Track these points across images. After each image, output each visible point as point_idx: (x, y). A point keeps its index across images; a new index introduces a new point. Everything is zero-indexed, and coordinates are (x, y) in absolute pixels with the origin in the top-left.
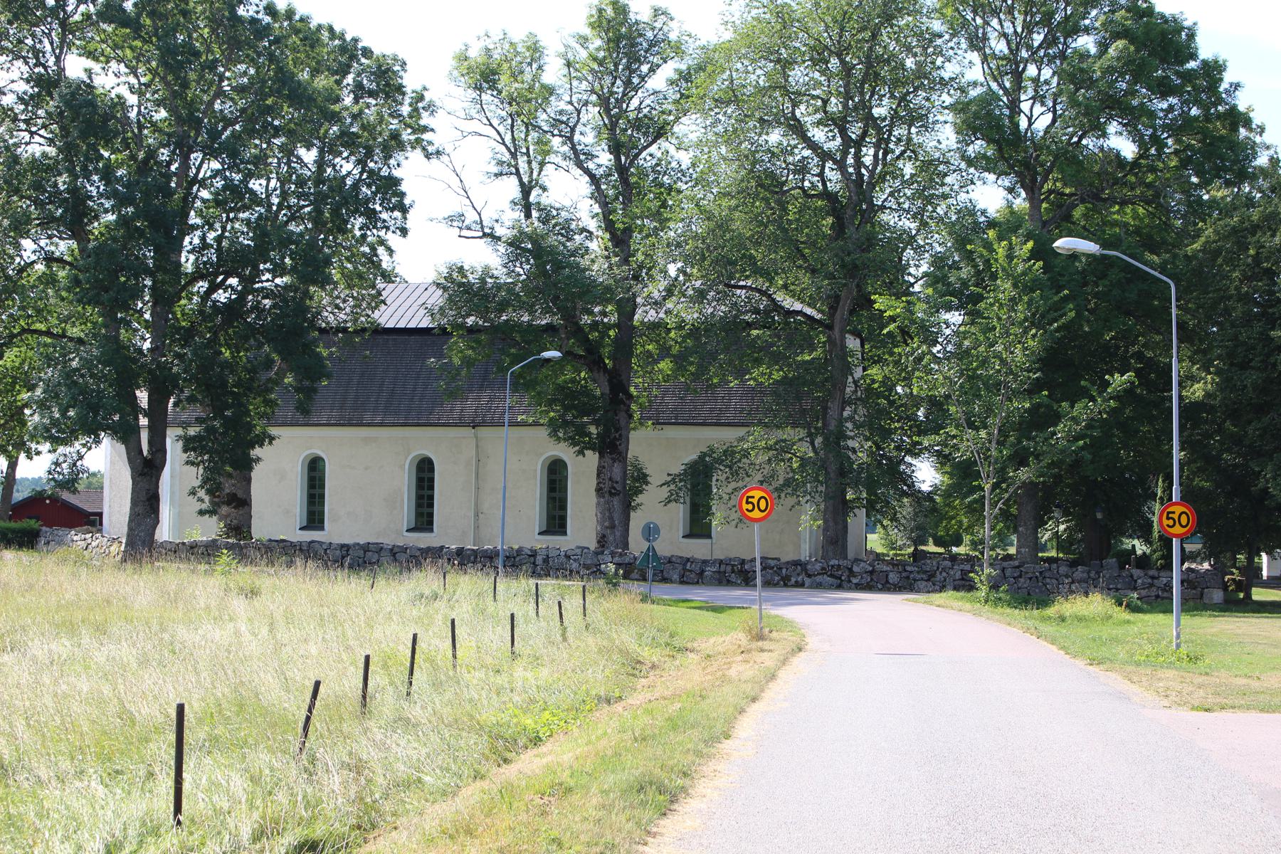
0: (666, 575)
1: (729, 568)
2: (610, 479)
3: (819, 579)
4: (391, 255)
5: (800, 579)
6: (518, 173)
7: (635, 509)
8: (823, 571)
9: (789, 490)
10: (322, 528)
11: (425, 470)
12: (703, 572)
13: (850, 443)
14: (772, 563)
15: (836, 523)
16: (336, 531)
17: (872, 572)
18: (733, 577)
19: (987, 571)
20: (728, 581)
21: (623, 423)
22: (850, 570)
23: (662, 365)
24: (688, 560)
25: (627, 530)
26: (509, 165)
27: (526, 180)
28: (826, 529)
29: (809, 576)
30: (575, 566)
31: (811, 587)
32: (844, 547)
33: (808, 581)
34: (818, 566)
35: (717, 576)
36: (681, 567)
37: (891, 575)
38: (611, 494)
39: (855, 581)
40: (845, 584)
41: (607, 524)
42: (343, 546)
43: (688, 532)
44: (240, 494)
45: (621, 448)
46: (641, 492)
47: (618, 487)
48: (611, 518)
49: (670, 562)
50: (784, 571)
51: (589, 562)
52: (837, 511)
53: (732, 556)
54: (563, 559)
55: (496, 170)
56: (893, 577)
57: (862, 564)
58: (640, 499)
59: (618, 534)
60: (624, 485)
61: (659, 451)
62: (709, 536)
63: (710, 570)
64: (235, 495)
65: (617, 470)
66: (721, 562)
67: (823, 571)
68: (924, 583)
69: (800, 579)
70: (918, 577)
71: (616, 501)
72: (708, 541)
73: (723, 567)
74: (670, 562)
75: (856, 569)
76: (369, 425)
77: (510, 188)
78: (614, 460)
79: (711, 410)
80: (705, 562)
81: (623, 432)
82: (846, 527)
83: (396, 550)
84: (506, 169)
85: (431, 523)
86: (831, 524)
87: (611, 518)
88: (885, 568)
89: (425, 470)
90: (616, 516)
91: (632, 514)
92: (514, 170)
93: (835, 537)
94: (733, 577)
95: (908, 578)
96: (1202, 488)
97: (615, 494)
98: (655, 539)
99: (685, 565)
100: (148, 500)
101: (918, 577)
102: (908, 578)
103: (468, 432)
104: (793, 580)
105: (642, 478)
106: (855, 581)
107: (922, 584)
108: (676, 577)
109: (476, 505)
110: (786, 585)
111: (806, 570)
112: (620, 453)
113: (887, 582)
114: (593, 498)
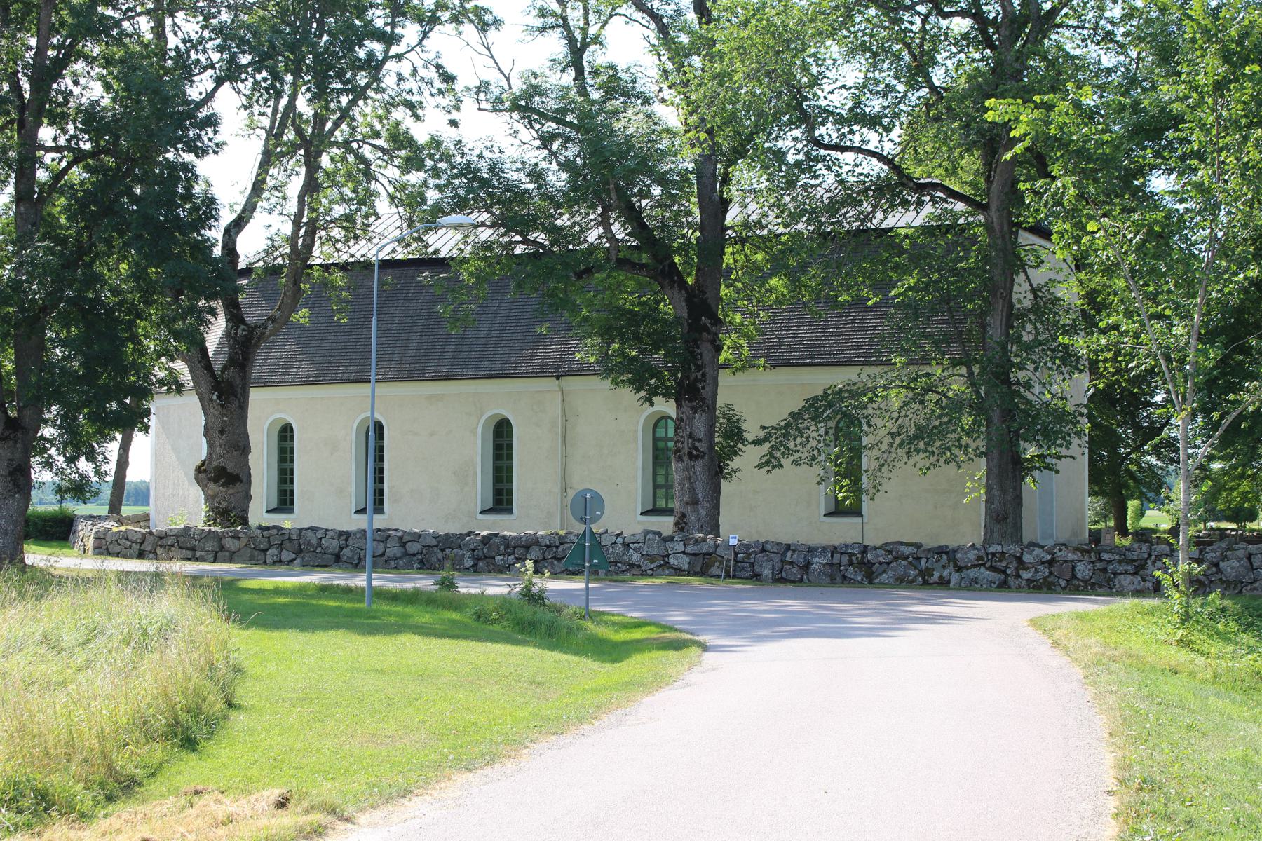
0: (758, 570)
1: (845, 559)
2: (691, 436)
3: (973, 573)
5: (945, 573)
6: (566, 25)
7: (728, 477)
8: (980, 562)
9: (921, 445)
10: (291, 511)
11: (502, 432)
12: (808, 564)
13: (1021, 375)
14: (906, 551)
16: (403, 514)
17: (1050, 563)
18: (851, 572)
19: (1183, 566)
20: (845, 577)
21: (707, 357)
22: (1019, 559)
23: (774, 281)
24: (788, 547)
25: (716, 507)
26: (554, 14)
27: (578, 34)
28: (989, 501)
29: (959, 569)
30: (635, 558)
31: (959, 588)
32: (1018, 527)
33: (955, 578)
34: (972, 555)
35: (828, 570)
36: (777, 558)
38: (691, 456)
39: (1026, 575)
40: (1012, 582)
41: (686, 498)
42: (341, 533)
44: (231, 468)
45: (706, 393)
46: (736, 453)
47: (702, 447)
48: (692, 490)
49: (763, 551)
50: (923, 562)
52: (1009, 472)
53: (849, 541)
55: (539, 22)
56: (1083, 570)
57: (1037, 551)
58: (735, 463)
59: (702, 512)
60: (711, 445)
61: (755, 396)
62: (858, 513)
63: (818, 562)
64: (223, 469)
65: (699, 424)
66: (834, 550)
67: (980, 562)
68: (1129, 578)
69: (945, 573)
70: (1120, 568)
71: (699, 466)
72: (858, 520)
73: (836, 556)
74: (763, 551)
75: (1027, 558)
76: (432, 379)
77: (555, 44)
78: (695, 410)
79: (859, 345)
80: (811, 550)
81: (708, 371)
83: (406, 538)
84: (551, 20)
85: (510, 502)
86: (997, 493)
87: (692, 490)
88: (1071, 556)
89: (502, 432)
90: (701, 488)
91: (724, 485)
92: (561, 22)
93: (1005, 512)
94: (851, 572)
95: (1105, 570)
97: (697, 457)
98: (595, 519)
99: (784, 554)
100: (11, 474)
101: (1120, 568)
102: (1105, 570)
103: (551, 383)
104: (936, 575)
105: (735, 433)
106: (1026, 575)
107: (1125, 580)
108: (767, 572)
109: (564, 478)
110: (926, 583)
111: (955, 561)
112: (703, 400)
113: (1074, 577)
114: (253, 440)
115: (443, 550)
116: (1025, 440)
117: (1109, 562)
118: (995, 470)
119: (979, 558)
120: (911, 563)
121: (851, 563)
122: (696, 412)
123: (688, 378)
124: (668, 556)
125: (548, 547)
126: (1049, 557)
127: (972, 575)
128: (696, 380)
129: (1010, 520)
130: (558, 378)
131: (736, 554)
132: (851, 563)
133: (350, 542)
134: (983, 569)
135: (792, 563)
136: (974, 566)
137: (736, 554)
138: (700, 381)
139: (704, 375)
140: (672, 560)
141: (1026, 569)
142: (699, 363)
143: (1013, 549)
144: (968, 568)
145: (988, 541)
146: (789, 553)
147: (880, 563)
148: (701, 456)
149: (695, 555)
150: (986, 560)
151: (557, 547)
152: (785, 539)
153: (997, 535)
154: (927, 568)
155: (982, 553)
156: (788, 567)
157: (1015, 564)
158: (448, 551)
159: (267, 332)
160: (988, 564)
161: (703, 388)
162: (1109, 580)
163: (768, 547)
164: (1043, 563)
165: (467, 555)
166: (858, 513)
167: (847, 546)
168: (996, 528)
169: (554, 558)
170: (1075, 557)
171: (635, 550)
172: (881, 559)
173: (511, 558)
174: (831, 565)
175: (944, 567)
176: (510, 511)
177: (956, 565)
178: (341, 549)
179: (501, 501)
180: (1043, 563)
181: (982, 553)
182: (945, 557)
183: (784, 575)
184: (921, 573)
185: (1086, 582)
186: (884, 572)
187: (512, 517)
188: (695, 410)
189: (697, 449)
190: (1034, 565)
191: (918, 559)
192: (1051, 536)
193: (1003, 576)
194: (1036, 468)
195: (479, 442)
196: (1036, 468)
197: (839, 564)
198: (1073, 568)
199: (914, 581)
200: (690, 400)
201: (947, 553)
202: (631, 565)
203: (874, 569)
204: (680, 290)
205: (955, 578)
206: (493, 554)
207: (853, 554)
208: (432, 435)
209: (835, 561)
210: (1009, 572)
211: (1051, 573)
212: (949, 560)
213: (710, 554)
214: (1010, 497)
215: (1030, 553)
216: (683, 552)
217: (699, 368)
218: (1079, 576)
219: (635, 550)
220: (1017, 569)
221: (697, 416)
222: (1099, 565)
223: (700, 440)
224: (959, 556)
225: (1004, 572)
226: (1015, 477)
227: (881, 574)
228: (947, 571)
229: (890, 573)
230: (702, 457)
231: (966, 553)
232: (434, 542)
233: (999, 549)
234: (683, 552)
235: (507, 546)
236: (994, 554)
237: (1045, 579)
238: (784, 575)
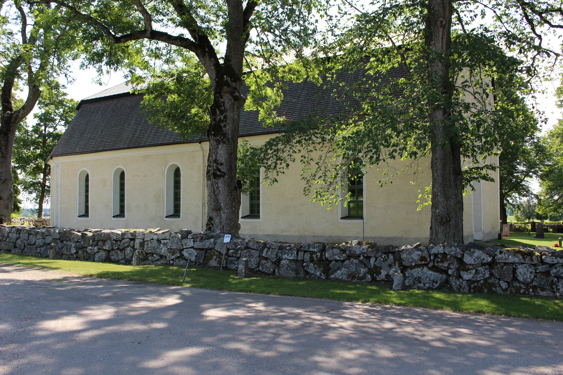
1: (307, 256)
3: (416, 272)
4: (483, 17)
8: (423, 262)
12: (280, 260)
15: (447, 198)
17: (491, 265)
18: (311, 268)
20: (307, 273)
22: (460, 261)
28: (434, 206)
32: (459, 227)
34: (416, 255)
35: (294, 266)
36: (256, 254)
37: (521, 270)
39: (467, 276)
43: (248, 213)
47: (224, 169)
48: (216, 200)
49: (247, 248)
50: (372, 261)
51: (174, 247)
54: (155, 243)
57: (478, 253)
59: (224, 216)
62: (361, 217)
67: (423, 262)
71: (221, 183)
72: (361, 221)
74: (247, 248)
75: (467, 259)
78: (218, 142)
82: (460, 203)
86: (441, 199)
87: (216, 200)
88: (511, 259)
90: (223, 199)
94: (311, 268)
95: (547, 273)
96: (279, 122)
97: (220, 176)
99: (261, 251)
104: (383, 273)
106: (467, 276)
111: (400, 260)
113: (515, 279)
115: (62, 242)
116: (465, 155)
117: (552, 265)
118: (439, 180)
119: (422, 258)
120: (361, 262)
121: (312, 260)
122: (219, 143)
123: (215, 120)
124: (183, 250)
125: (116, 241)
126: (490, 259)
127: (415, 275)
128: (220, 121)
129: (453, 221)
130: (200, 143)
131: (228, 250)
132: (312, 260)
133: (21, 235)
134: (425, 269)
135: (266, 259)
136: (417, 266)
137: (228, 250)
138: (223, 121)
139: (225, 117)
140: (185, 253)
141: (467, 270)
142: (222, 108)
143: (454, 251)
144: (412, 268)
145: (433, 240)
146: (266, 250)
147: (336, 261)
148: (223, 175)
149: (201, 249)
150: (429, 260)
151: (121, 241)
152: (77, 262)
153: (441, 236)
154: (375, 266)
155: (425, 254)
156: (264, 262)
157: (455, 265)
158: (65, 242)
159: (20, 115)
160: (431, 265)
161: (225, 126)
162: (552, 283)
163: (251, 245)
164: (483, 264)
165: (73, 245)
166: (361, 217)
167: (309, 245)
168: (441, 229)
169: (118, 249)
170: (516, 260)
171: (164, 244)
172: (337, 257)
173: (96, 248)
174: (296, 261)
175: (390, 266)
176: (258, 217)
177: (401, 265)
178: (17, 239)
179: (354, 212)
180: (483, 264)
181: (425, 254)
182: (391, 257)
183: (261, 268)
184: (370, 271)
185: (527, 285)
186: (339, 269)
187: (180, 219)
188: (218, 142)
189: (219, 170)
190: (475, 267)
191: (368, 258)
192: (481, 230)
193: (444, 276)
194: (474, 178)
195: (165, 179)
196: (474, 178)
197: (303, 261)
198: (514, 270)
199: (364, 277)
200: (215, 135)
201: (393, 253)
202: (161, 256)
203: (331, 265)
204: (210, 58)
205: (397, 277)
206: (86, 245)
207: (314, 253)
208: (145, 176)
209: (300, 258)
210: (450, 272)
211: (491, 275)
212: (395, 259)
213: (211, 249)
214: (452, 202)
215: (471, 255)
216: (192, 247)
217: (222, 112)
218: (520, 278)
219: (164, 244)
220: (458, 270)
221: (220, 146)
222: (540, 268)
223: (222, 164)
224: (404, 256)
225: (446, 272)
226: (456, 185)
227: (336, 271)
228: (393, 269)
229: (344, 270)
230: (223, 177)
231: (410, 254)
232: (58, 237)
233: (441, 250)
234: (192, 247)
235: (94, 241)
236: (436, 255)
237: (485, 280)
238: (261, 268)
